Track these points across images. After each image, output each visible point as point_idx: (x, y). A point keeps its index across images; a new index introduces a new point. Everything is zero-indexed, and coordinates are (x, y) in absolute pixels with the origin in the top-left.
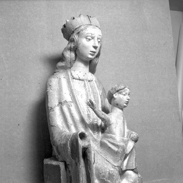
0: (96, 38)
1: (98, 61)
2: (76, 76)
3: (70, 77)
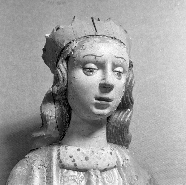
0: (109, 67)
2: (68, 162)
3: (55, 161)
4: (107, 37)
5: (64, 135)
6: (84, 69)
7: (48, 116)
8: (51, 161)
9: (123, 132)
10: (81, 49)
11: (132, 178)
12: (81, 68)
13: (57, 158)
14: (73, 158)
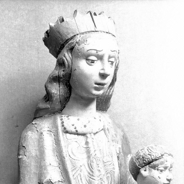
0: (106, 58)
1: (113, 91)
2: (71, 128)
3: (60, 129)
4: (104, 32)
5: (64, 107)
6: (87, 60)
7: (54, 93)
8: (57, 127)
9: (107, 102)
10: (85, 43)
11: (113, 136)
12: (84, 58)
13: (61, 125)
14: (75, 126)
